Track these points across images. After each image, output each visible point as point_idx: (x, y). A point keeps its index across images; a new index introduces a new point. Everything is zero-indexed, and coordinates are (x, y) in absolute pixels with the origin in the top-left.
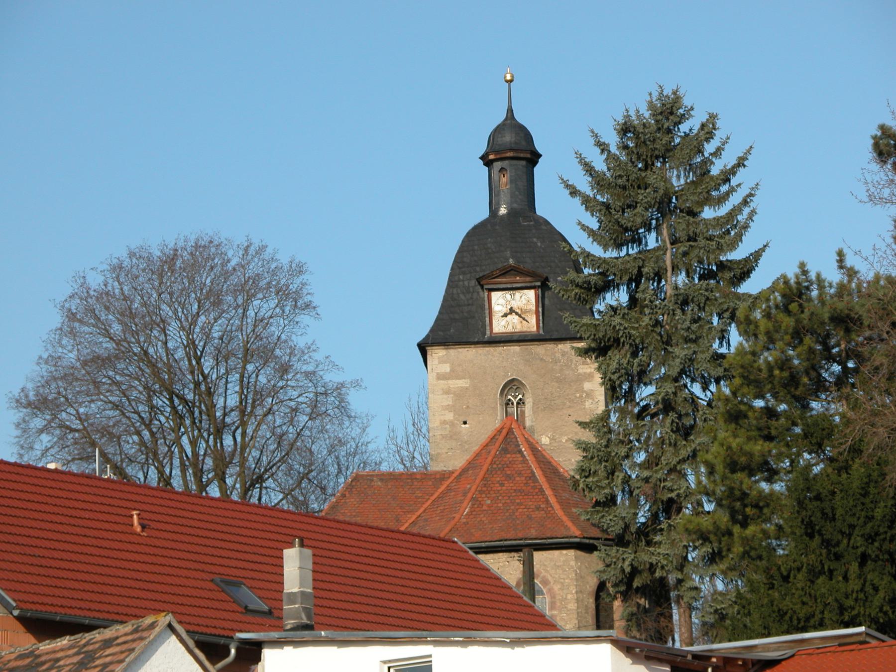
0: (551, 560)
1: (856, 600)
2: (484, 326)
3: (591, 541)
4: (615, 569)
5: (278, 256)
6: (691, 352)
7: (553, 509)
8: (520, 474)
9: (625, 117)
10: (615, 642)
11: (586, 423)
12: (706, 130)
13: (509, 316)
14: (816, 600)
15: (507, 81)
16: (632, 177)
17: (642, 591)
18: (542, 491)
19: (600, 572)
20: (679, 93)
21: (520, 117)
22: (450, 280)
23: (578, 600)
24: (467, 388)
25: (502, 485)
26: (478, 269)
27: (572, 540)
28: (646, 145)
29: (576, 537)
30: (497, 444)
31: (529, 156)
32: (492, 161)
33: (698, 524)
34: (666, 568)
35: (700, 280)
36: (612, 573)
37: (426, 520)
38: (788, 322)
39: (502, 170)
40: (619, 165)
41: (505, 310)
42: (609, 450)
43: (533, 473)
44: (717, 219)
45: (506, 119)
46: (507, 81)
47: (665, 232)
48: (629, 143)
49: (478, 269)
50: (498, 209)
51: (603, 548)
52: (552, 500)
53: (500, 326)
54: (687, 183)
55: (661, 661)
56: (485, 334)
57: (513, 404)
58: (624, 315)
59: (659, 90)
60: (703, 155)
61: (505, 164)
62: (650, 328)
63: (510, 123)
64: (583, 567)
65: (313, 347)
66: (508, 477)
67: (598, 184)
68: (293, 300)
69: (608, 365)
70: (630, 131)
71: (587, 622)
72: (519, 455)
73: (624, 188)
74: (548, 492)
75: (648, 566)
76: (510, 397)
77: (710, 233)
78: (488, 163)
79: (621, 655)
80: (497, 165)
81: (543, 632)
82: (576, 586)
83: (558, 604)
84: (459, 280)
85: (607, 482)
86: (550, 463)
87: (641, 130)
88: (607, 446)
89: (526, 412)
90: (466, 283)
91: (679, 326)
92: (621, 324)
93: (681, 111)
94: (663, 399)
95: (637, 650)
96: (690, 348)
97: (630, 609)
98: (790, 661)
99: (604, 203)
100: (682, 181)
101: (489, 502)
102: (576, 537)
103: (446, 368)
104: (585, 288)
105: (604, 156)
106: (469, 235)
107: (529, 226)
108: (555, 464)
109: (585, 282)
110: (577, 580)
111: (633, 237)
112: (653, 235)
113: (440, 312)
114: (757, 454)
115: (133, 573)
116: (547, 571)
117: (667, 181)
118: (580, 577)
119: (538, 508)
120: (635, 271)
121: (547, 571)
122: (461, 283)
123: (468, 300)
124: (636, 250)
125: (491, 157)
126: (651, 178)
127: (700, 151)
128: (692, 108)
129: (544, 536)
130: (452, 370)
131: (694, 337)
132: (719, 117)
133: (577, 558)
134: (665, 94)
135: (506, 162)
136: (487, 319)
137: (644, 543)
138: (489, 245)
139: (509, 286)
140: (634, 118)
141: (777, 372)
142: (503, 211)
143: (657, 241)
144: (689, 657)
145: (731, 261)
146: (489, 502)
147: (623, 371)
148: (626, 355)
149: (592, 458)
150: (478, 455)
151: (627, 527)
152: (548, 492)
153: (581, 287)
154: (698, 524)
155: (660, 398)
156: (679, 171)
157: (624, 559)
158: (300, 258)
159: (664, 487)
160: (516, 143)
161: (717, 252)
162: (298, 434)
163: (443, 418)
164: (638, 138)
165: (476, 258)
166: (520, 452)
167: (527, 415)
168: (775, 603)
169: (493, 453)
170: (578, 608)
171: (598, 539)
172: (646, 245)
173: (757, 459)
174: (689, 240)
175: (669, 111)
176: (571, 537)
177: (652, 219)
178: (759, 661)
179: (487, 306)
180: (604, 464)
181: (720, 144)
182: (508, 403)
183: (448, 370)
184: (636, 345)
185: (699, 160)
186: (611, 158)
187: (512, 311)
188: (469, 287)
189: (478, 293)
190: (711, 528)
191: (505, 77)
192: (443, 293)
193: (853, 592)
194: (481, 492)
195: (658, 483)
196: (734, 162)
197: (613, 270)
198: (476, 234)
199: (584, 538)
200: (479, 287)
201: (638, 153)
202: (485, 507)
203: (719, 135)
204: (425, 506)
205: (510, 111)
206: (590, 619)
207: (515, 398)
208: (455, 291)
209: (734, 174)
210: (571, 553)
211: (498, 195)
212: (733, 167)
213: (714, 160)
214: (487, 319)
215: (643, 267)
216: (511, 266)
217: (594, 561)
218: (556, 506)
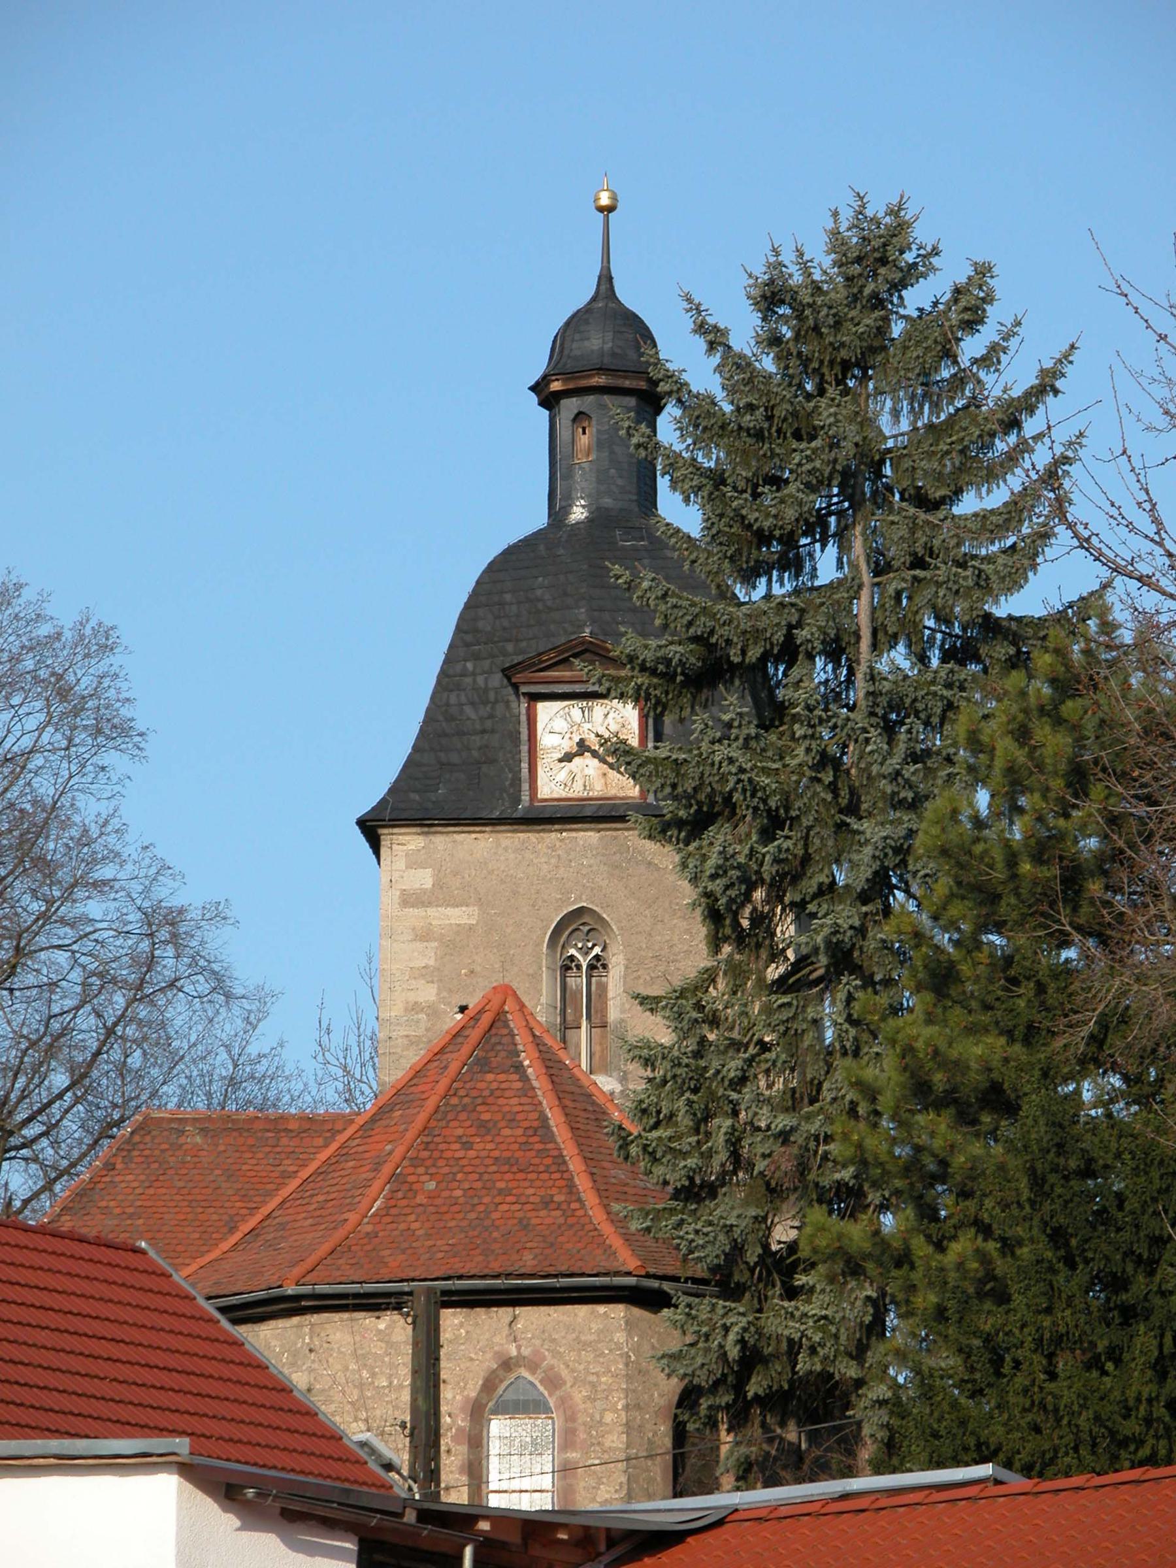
1: (1148, 1421)
2: (517, 781)
3: (655, 1284)
4: (707, 1350)
5: (49, 610)
6: (901, 831)
7: (583, 1206)
8: (512, 1122)
9: (769, 265)
10: (186, 1470)
11: (657, 999)
12: (963, 303)
13: (577, 760)
14: (1058, 1420)
15: (601, 209)
16: (780, 412)
17: (778, 1403)
19: (672, 1357)
20: (907, 215)
21: (628, 295)
22: (444, 674)
23: (628, 1427)
24: (471, 928)
25: (467, 1146)
26: (510, 647)
28: (821, 335)
29: (629, 1274)
30: (466, 1049)
32: (559, 395)
33: (840, 1236)
34: (821, 1352)
35: (944, 660)
36: (699, 1361)
37: (282, 1226)
38: (1053, 743)
39: (579, 416)
40: (750, 381)
41: (568, 745)
42: (703, 1063)
43: (544, 1119)
44: (982, 517)
45: (594, 299)
46: (601, 209)
47: (858, 546)
48: (784, 329)
49: (510, 647)
50: (566, 510)
51: (684, 1300)
52: (583, 1183)
53: (554, 782)
54: (916, 429)
55: (329, 1524)
56: (519, 801)
57: (579, 967)
58: (748, 739)
59: (856, 205)
60: (955, 362)
61: (587, 402)
62: (808, 773)
63: (606, 311)
65: (115, 823)
66: (484, 1127)
67: (696, 426)
68: (89, 717)
69: (704, 858)
70: (783, 302)
71: (651, 1481)
72: (516, 1077)
73: (759, 435)
74: (575, 1165)
75: (784, 1346)
76: (572, 951)
77: (965, 549)
78: (549, 400)
79: (208, 1507)
80: (570, 406)
81: (13, 1443)
82: (626, 1391)
83: (583, 1436)
84: (463, 674)
85: (693, 1139)
86: (590, 1096)
87: (808, 300)
88: (698, 1055)
89: (610, 987)
90: (480, 680)
91: (875, 769)
92: (731, 761)
93: (909, 257)
94: (828, 942)
95: (250, 1492)
96: (899, 821)
97: (743, 1450)
98: (708, 1537)
99: (710, 470)
100: (905, 425)
101: (432, 1185)
102: (629, 1274)
103: (424, 879)
104: (663, 675)
105: (716, 359)
106: (492, 568)
107: (635, 549)
108: (601, 1100)
109: (658, 661)
110: (629, 1378)
111: (783, 555)
112: (832, 550)
113: (416, 748)
114: (974, 1065)
115: (252, 1410)
116: (556, 1354)
117: (867, 422)
118: (634, 1372)
119: (547, 1203)
120: (779, 637)
121: (556, 1354)
122: (468, 680)
123: (482, 719)
124: (788, 587)
125: (556, 386)
126: (825, 413)
127: (949, 354)
128: (935, 252)
129: (552, 1270)
130: (438, 884)
131: (910, 795)
132: (995, 271)
133: (630, 1325)
134: (869, 213)
135: (590, 399)
136: (525, 765)
137: (778, 1290)
138: (539, 592)
139: (578, 688)
140: (793, 269)
141: (1026, 867)
142: (578, 513)
143: (840, 565)
144: (410, 1517)
145: (1019, 620)
146: (432, 1185)
147: (734, 873)
148: (748, 835)
149: (665, 1082)
150: (418, 1073)
151: (737, 1249)
152: (575, 1165)
153: (653, 672)
154: (840, 1236)
155: (819, 939)
156: (896, 401)
157: (726, 1329)
158: (104, 614)
159: (825, 1157)
160: (614, 355)
161: (977, 594)
162: (110, 1032)
163: (412, 997)
164: (800, 317)
165: (506, 623)
166: (519, 1068)
167: (610, 994)
168: (970, 1427)
169: (454, 1067)
170: (629, 1445)
171: (675, 1279)
172: (814, 575)
173: (975, 1078)
174: (913, 566)
175: (878, 256)
176: (617, 1274)
177: (830, 514)
178: (631, 1534)
179: (524, 736)
180: (687, 1095)
181: (997, 338)
182: (569, 965)
183: (428, 884)
184: (769, 811)
185: (946, 374)
186: (736, 368)
187: (583, 748)
188: (486, 690)
189: (507, 703)
190: (867, 1246)
191: (597, 199)
192: (425, 702)
193: (1138, 1400)
194: (416, 1162)
195: (812, 1145)
196: (1031, 380)
197: (724, 631)
199: (648, 1276)
200: (510, 690)
201: (800, 354)
202: (420, 1199)
203: (997, 315)
204: (284, 1193)
205: (606, 279)
206: (659, 1471)
207: (587, 954)
208: (453, 699)
209: (1031, 410)
210: (617, 1312)
211: (568, 476)
212: (1028, 394)
213: (982, 375)
214: (525, 765)
215: (799, 625)
216: (583, 642)
217: (662, 1330)
218: (590, 1199)
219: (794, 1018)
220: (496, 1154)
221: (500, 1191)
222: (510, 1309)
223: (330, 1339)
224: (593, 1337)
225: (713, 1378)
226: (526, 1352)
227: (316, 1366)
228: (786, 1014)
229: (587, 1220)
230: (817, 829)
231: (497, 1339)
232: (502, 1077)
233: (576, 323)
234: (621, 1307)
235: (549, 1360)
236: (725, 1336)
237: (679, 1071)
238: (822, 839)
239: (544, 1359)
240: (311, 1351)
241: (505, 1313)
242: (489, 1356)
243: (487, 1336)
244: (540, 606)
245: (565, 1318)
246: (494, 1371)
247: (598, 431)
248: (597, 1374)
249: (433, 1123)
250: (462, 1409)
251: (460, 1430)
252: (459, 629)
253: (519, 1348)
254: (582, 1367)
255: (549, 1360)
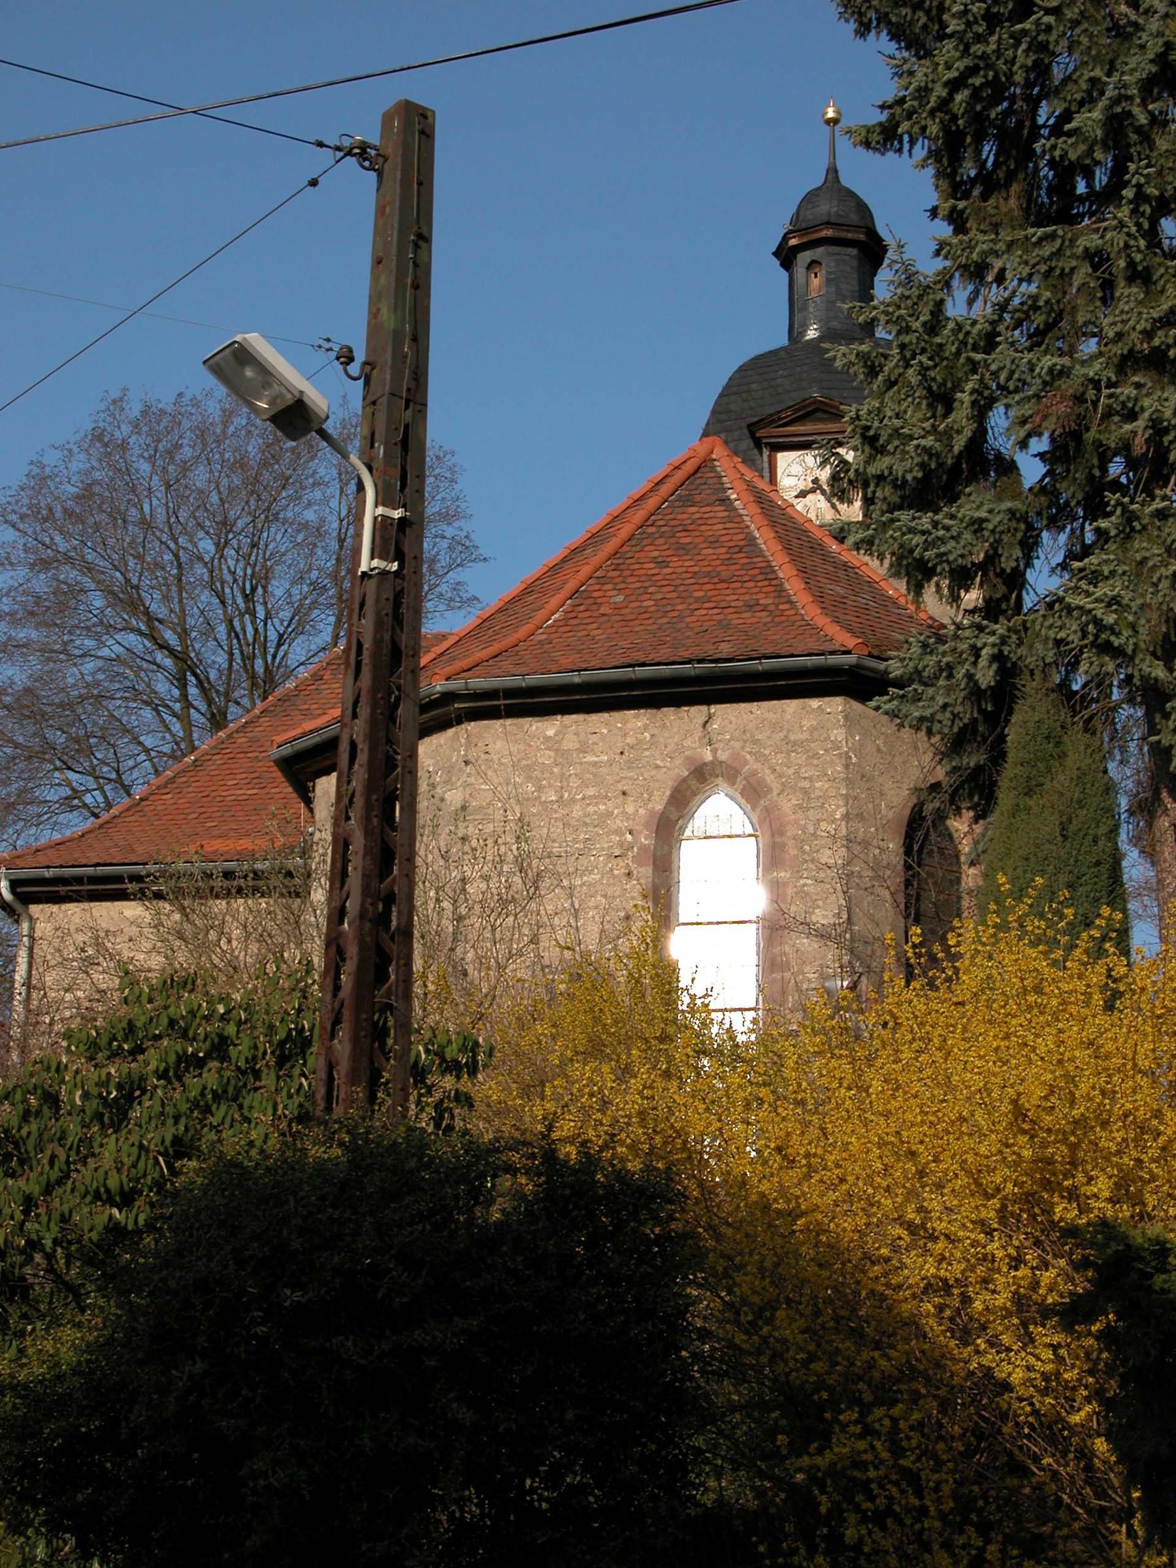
0: (774, 726)
8: (714, 543)
13: (810, 496)
18: (768, 572)
21: (846, 181)
27: (833, 660)
31: (862, 237)
36: (940, 701)
46: (828, 122)
50: (803, 333)
61: (818, 253)
64: (870, 748)
80: (804, 257)
82: (846, 797)
106: (741, 369)
110: (849, 782)
116: (760, 757)
118: (857, 776)
121: (760, 757)
125: (793, 242)
133: (850, 722)
135: (821, 250)
166: (725, 501)
198: (758, 367)
205: (833, 171)
210: (836, 705)
211: (804, 308)
219: (1059, 253)
220: (696, 569)
221: (697, 600)
222: (704, 708)
223: (490, 748)
224: (804, 736)
225: (959, 724)
226: (723, 756)
227: (472, 780)
228: (1047, 250)
229: (798, 618)
230: (1085, 25)
231: (688, 743)
232: (707, 509)
233: (810, 198)
234: (839, 700)
235: (752, 764)
236: (975, 663)
237: (906, 339)
238: (1091, 36)
239: (746, 762)
240: (466, 763)
241: (698, 712)
242: (678, 762)
243: (676, 738)
244: (780, 390)
245: (771, 715)
246: (684, 780)
247: (828, 273)
248: (810, 779)
249: (625, 549)
250: (646, 825)
251: (642, 848)
252: (714, 412)
253: (714, 752)
254: (791, 771)
255: (752, 764)
